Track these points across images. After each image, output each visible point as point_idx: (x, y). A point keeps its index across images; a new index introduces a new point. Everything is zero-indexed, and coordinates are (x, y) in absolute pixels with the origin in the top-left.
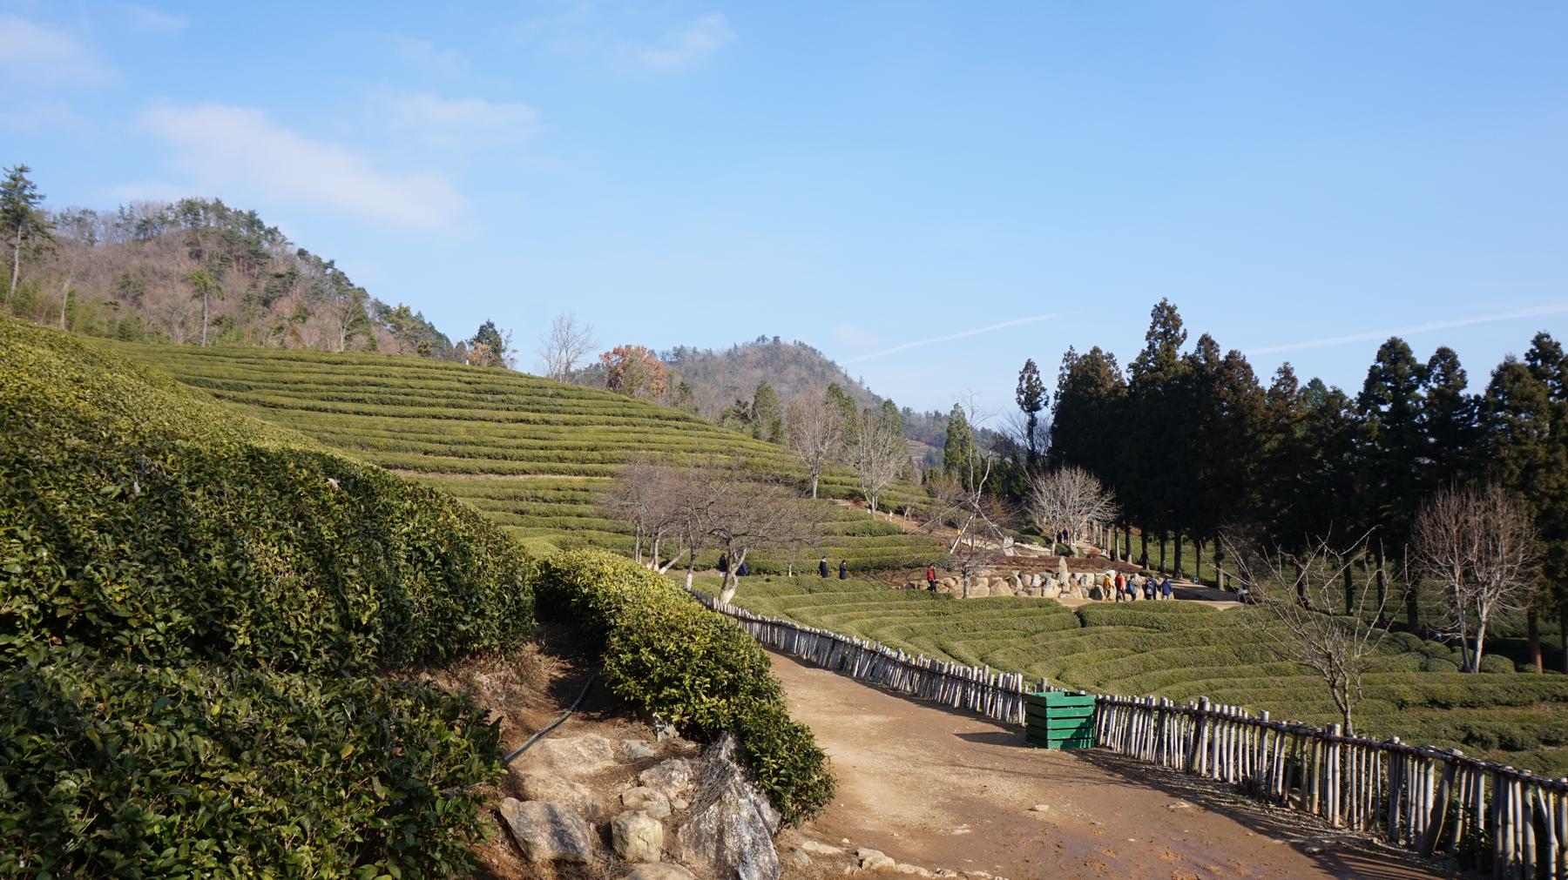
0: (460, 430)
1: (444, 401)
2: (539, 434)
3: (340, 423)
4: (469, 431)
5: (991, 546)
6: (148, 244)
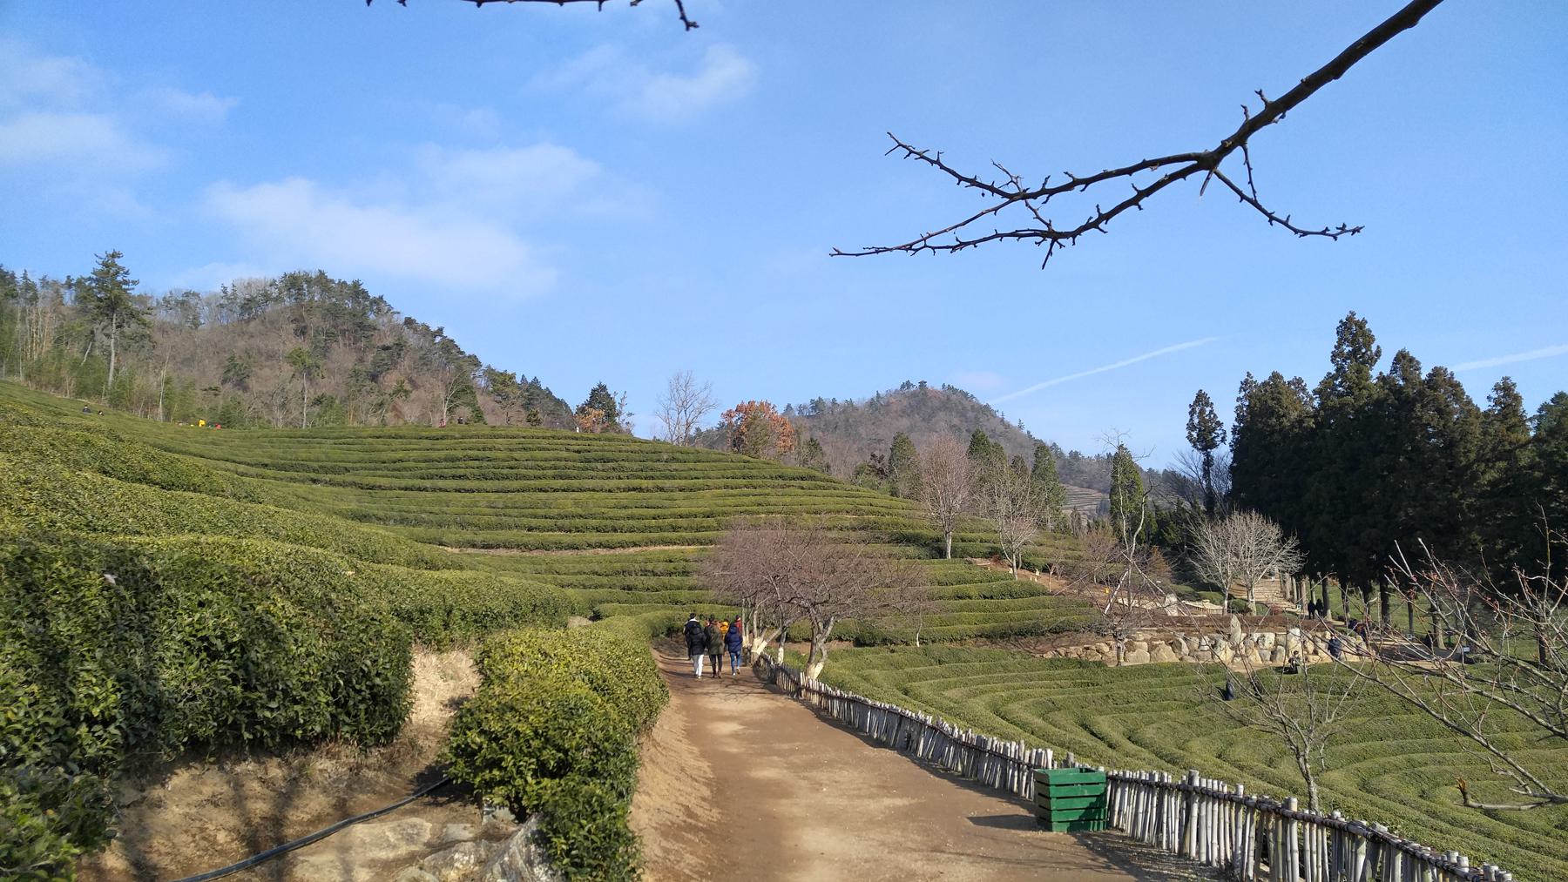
0: (567, 502)
1: (550, 473)
2: (653, 502)
3: (439, 502)
4: (577, 503)
5: (1149, 605)
6: (252, 324)
